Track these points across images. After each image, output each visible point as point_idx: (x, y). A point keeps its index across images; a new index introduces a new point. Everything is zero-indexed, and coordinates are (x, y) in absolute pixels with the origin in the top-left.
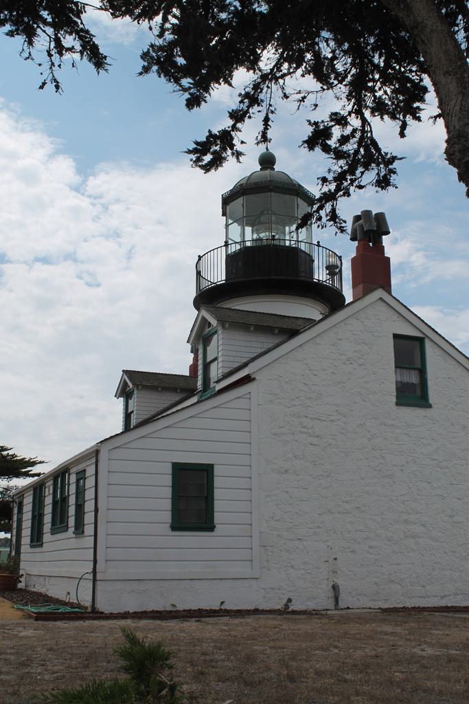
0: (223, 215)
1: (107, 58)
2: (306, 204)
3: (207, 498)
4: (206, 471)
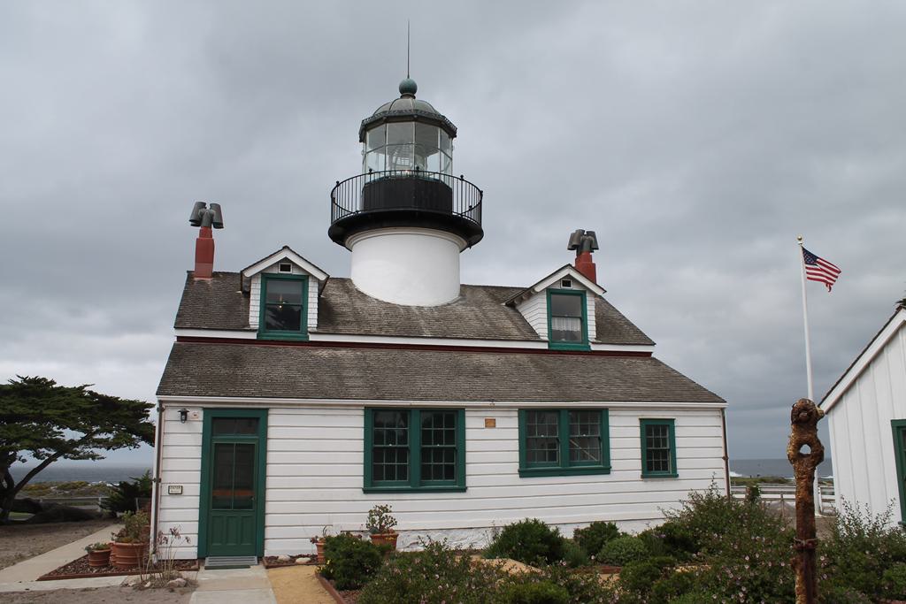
0: (360, 141)
1: (482, 424)
2: (447, 135)
3: (421, 411)
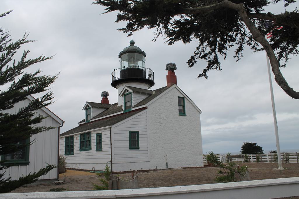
4: (137, 133)
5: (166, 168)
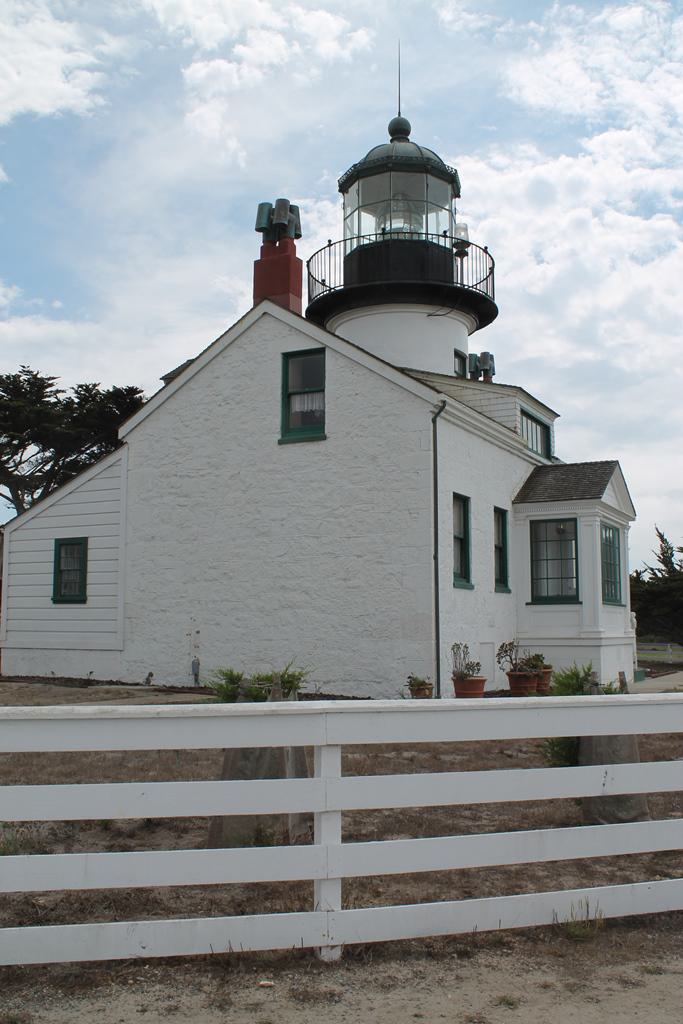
5: (191, 683)
